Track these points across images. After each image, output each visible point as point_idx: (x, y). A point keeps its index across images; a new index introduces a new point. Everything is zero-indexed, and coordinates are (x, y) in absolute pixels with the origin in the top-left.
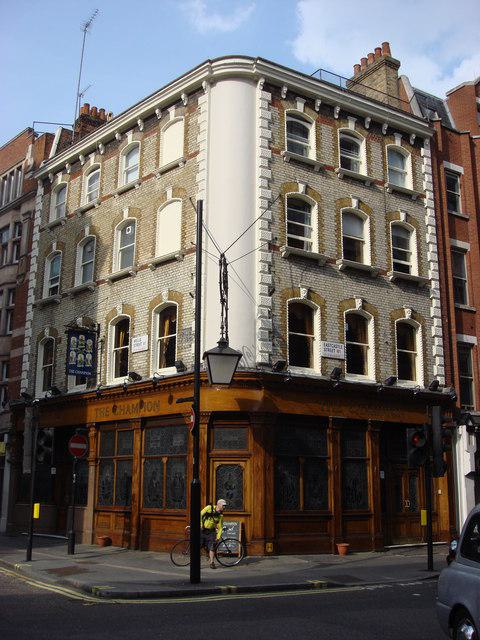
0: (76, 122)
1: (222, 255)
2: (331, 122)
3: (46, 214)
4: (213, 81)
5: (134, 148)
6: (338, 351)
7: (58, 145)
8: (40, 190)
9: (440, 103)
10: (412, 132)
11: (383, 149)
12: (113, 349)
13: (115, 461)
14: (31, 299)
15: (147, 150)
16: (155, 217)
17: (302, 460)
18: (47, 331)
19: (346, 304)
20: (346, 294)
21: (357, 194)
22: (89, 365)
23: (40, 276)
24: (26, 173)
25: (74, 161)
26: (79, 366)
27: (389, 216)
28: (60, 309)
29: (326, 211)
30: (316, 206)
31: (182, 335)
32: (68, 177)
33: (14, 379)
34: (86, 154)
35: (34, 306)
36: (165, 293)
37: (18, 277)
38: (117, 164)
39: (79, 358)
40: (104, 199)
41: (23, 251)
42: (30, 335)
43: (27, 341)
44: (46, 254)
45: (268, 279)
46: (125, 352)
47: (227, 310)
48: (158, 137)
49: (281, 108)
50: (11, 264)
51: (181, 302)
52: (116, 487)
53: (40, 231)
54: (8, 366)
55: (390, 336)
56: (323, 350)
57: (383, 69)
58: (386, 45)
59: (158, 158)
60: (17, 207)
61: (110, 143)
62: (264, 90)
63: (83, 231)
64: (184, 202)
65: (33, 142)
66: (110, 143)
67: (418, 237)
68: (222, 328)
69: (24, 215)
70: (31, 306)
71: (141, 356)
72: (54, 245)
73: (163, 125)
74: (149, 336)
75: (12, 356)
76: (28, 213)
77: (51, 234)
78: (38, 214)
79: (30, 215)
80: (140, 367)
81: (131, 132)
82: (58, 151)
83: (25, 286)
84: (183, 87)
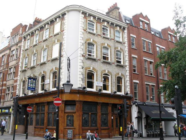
2: (100, 23)
3: (24, 47)
4: (68, 11)
8: (23, 40)
9: (131, 19)
13: (40, 114)
14: (20, 69)
15: (51, 29)
17: (90, 114)
18: (23, 78)
20: (103, 69)
22: (34, 87)
23: (22, 63)
24: (20, 35)
27: (115, 48)
35: (20, 71)
36: (54, 68)
37: (16, 63)
41: (18, 57)
43: (18, 81)
45: (82, 64)
46: (43, 84)
47: (70, 72)
48: (54, 26)
49: (87, 19)
50: (15, 60)
53: (23, 51)
55: (114, 80)
56: (98, 83)
58: (116, 3)
59: (53, 32)
63: (34, 51)
65: (22, 27)
66: (42, 28)
67: (123, 54)
68: (68, 77)
72: (35, 51)
73: (55, 23)
76: (20, 46)
79: (20, 47)
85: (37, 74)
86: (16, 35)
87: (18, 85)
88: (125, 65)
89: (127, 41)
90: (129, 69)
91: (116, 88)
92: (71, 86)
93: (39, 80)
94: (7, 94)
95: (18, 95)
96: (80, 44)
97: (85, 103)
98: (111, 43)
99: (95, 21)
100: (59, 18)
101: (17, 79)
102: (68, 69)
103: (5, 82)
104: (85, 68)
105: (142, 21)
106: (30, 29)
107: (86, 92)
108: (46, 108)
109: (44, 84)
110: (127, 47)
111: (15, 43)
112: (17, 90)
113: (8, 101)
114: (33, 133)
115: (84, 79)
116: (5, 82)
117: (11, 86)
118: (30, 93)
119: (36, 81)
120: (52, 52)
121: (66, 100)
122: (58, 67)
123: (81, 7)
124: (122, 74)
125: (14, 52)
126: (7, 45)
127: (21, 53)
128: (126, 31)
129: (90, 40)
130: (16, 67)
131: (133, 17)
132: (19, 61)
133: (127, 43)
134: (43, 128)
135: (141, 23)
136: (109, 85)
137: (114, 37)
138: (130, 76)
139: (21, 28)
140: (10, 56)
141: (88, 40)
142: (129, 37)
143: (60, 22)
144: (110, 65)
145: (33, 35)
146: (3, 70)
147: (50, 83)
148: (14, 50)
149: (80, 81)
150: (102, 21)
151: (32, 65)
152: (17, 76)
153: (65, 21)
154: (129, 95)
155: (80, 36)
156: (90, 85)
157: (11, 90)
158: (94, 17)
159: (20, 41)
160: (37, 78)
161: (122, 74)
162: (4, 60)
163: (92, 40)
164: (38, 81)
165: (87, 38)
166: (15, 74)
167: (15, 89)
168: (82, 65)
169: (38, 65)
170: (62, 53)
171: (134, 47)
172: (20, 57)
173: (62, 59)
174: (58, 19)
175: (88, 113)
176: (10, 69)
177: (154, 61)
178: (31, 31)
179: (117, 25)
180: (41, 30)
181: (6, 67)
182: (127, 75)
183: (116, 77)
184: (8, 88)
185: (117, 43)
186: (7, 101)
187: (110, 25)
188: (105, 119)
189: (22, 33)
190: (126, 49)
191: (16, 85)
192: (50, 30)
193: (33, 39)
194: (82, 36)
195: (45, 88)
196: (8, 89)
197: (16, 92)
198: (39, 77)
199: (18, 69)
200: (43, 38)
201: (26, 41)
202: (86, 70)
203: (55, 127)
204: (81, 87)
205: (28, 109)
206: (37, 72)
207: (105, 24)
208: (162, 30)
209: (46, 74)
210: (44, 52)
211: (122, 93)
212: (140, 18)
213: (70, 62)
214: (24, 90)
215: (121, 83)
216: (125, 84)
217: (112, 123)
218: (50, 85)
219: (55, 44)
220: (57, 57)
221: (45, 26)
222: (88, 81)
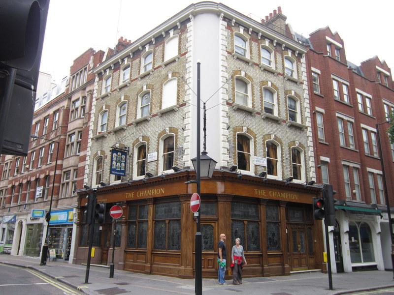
2: (257, 41)
3: (100, 91)
4: (195, 15)
6: (263, 162)
7: (107, 56)
8: (97, 79)
11: (282, 57)
13: (137, 223)
14: (91, 136)
15: (157, 54)
16: (162, 88)
17: (246, 222)
18: (99, 152)
20: (267, 131)
22: (123, 169)
23: (96, 124)
24: (89, 71)
26: (117, 169)
27: (286, 92)
28: (106, 140)
29: (255, 87)
31: (177, 151)
32: (112, 71)
33: (80, 179)
35: (92, 139)
36: (167, 129)
37: (84, 124)
40: (132, 81)
41: (87, 111)
42: (93, 129)
43: (88, 158)
44: (99, 111)
46: (144, 162)
48: (164, 46)
49: (232, 31)
50: (80, 118)
51: (177, 133)
53: (96, 100)
54: (80, 145)
55: (288, 155)
56: (257, 161)
58: (279, 8)
59: (163, 58)
62: (223, 20)
63: (121, 98)
64: (179, 79)
65: (94, 55)
69: (88, 92)
71: (153, 163)
72: (104, 107)
73: (166, 40)
75: (79, 166)
76: (90, 91)
78: (95, 92)
79: (91, 93)
80: (152, 170)
83: (87, 130)
86: (81, 72)
87: (87, 167)
88: (304, 124)
89: (306, 79)
90: (313, 134)
91: (291, 171)
93: (133, 154)
94: (63, 184)
95: (89, 186)
96: (221, 79)
97: (236, 200)
98: (278, 82)
99: (248, 37)
103: (59, 162)
104: (233, 128)
105: (330, 44)
107: (238, 176)
108: (151, 208)
109: (144, 161)
110: (306, 92)
111: (80, 85)
112: (86, 176)
113: (67, 198)
114: (120, 263)
115: (232, 150)
116: (59, 162)
117: (72, 169)
118: (114, 182)
119: (128, 157)
120: (161, 98)
124: (300, 144)
125: (78, 104)
126: (63, 90)
127: (93, 104)
128: (303, 60)
129: (239, 73)
130: (83, 132)
131: (312, 35)
132: (89, 120)
133: (305, 83)
134: (146, 252)
136: (277, 161)
138: (314, 148)
139: (92, 57)
140: (70, 111)
142: (309, 72)
145: (118, 67)
146: (57, 139)
147: (158, 160)
148: (78, 100)
149: (225, 154)
150: (260, 38)
151: (117, 125)
152: (86, 149)
153: (188, 35)
154: (315, 185)
155: (221, 63)
156: (243, 162)
157: (72, 177)
158: (246, 29)
159: (91, 82)
160: (128, 151)
161: (300, 144)
162: (57, 120)
163: (243, 74)
164: (132, 156)
165: (233, 68)
166: (82, 145)
167: (81, 174)
168: (228, 122)
169: (131, 124)
171: (318, 92)
172: (92, 112)
174: (172, 33)
175: (243, 221)
176: (69, 135)
177: (355, 90)
178: (113, 59)
180: (136, 56)
181: (62, 132)
182: (309, 145)
183: (290, 148)
184: (67, 173)
186: (64, 198)
187: (275, 47)
188: (273, 235)
190: (306, 95)
191: (84, 167)
193: (117, 75)
194: (226, 64)
195: (147, 171)
196: (67, 176)
197: (82, 180)
198: (133, 149)
199: (88, 134)
201: (121, 70)
202: (235, 132)
204: (227, 166)
205: (112, 212)
206: (129, 140)
208: (363, 64)
210: (142, 99)
211: (302, 181)
212: (328, 38)
214: (99, 177)
215: (297, 161)
216: (306, 164)
217: (288, 240)
218: (158, 164)
219: (167, 82)
220: (175, 106)
221: (144, 47)
222: (238, 153)
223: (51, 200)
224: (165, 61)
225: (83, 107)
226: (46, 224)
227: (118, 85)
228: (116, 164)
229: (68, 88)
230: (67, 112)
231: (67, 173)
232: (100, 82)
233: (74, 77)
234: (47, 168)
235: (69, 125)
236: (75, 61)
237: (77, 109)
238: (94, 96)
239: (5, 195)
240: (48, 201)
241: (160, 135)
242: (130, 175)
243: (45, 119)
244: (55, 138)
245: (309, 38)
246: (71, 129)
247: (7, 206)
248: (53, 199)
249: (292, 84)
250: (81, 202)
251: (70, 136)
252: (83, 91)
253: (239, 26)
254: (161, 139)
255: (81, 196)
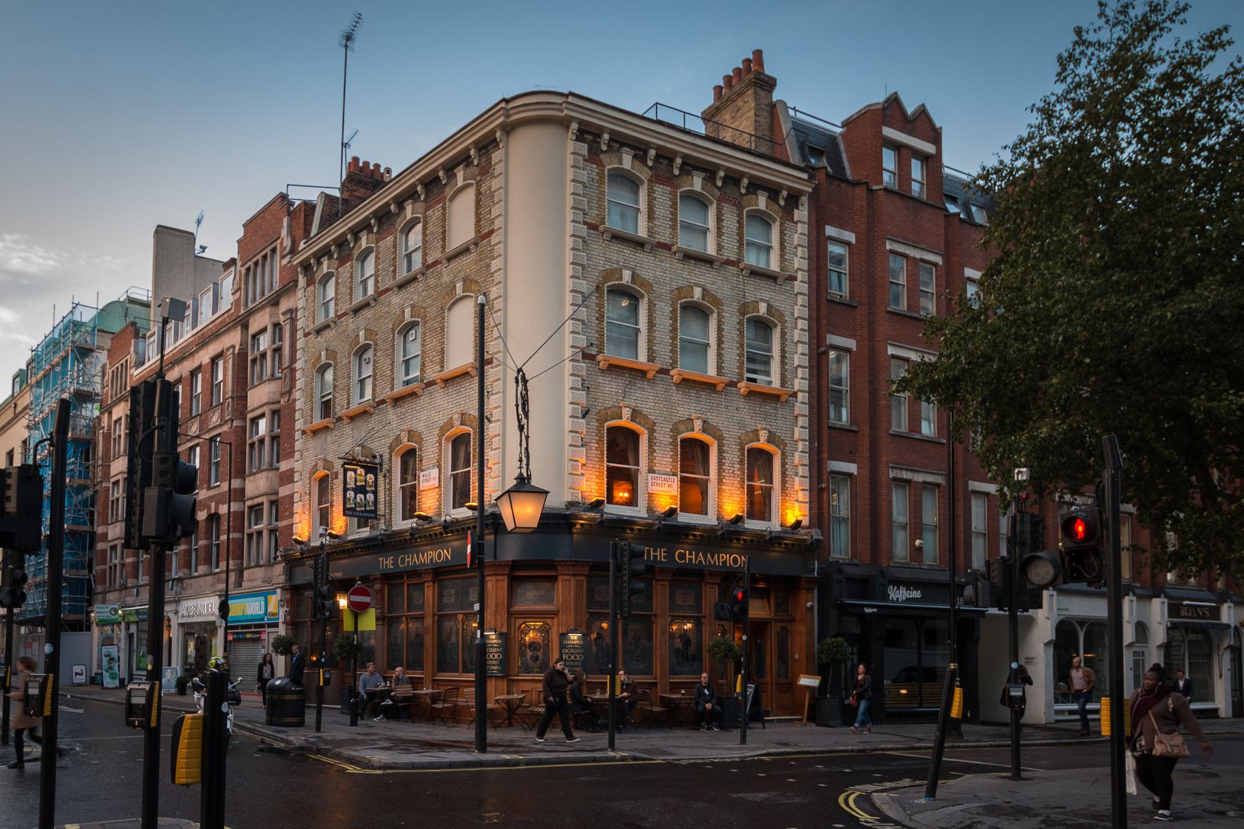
0: (343, 184)
1: (520, 370)
2: (669, 180)
4: (509, 129)
5: (368, 251)
8: (302, 281)
9: (832, 139)
10: (781, 186)
12: (399, 485)
14: (299, 425)
15: (430, 227)
19: (682, 427)
20: (683, 412)
21: (701, 280)
24: (283, 257)
25: (341, 243)
29: (659, 305)
30: (646, 299)
32: (335, 263)
34: (356, 232)
35: (304, 432)
37: (282, 395)
38: (395, 246)
39: (358, 500)
45: (582, 397)
47: (527, 437)
48: (444, 208)
49: (601, 164)
50: (273, 378)
52: (407, 648)
53: (306, 335)
54: (277, 507)
57: (750, 92)
58: (758, 54)
60: (274, 302)
61: (384, 217)
65: (289, 214)
66: (384, 217)
67: (783, 334)
68: (521, 460)
69: (284, 314)
70: (300, 432)
73: (449, 192)
74: (440, 471)
77: (319, 339)
79: (292, 312)
81: (410, 201)
82: (323, 226)
83: (291, 405)
84: (371, 210)
85: (380, 446)
86: (265, 257)
92: (545, 495)
93: (390, 471)
98: (722, 285)
99: (643, 174)
100: (467, 166)
101: (289, 467)
102: (519, 421)
103: (236, 483)
105: (898, 147)
106: (328, 220)
108: (429, 592)
111: (267, 294)
119: (381, 478)
121: (514, 561)
122: (474, 412)
123: (570, 99)
125: (265, 343)
128: (801, 214)
130: (281, 414)
132: (293, 386)
135: (889, 160)
137: (740, 253)
138: (810, 443)
139: (285, 220)
140: (250, 358)
141: (608, 275)
143: (471, 185)
144: (716, 391)
145: (346, 252)
146: (225, 428)
148: (264, 330)
159: (289, 288)
160: (381, 465)
164: (388, 475)
166: (281, 443)
170: (492, 346)
172: (298, 365)
173: (490, 372)
179: (756, 185)
180: (385, 227)
183: (742, 449)
185: (752, 281)
189: (294, 244)
191: (292, 496)
192: (425, 228)
198: (390, 459)
199: (293, 421)
200: (394, 271)
202: (601, 422)
203: (471, 677)
207: (692, 185)
209: (420, 442)
212: (888, 132)
213: (526, 390)
222: (608, 467)
223: (228, 571)
224: (447, 250)
225: (277, 351)
226: (221, 624)
227: (351, 300)
228: (355, 497)
229: (239, 299)
230: (241, 359)
231: (256, 510)
232: (311, 288)
233: (248, 269)
234: (211, 498)
235: (249, 393)
236: (246, 226)
237: (263, 355)
238: (300, 324)
239: (122, 559)
240: (221, 572)
241: (443, 430)
242: (387, 516)
243: (193, 373)
244: (221, 425)
245: (842, 134)
246: (255, 406)
247: (130, 582)
248: (230, 568)
249: (763, 283)
250: (511, 590)
251: (255, 421)
252: (273, 310)
253: (619, 149)
254: (447, 439)
255: (292, 563)
